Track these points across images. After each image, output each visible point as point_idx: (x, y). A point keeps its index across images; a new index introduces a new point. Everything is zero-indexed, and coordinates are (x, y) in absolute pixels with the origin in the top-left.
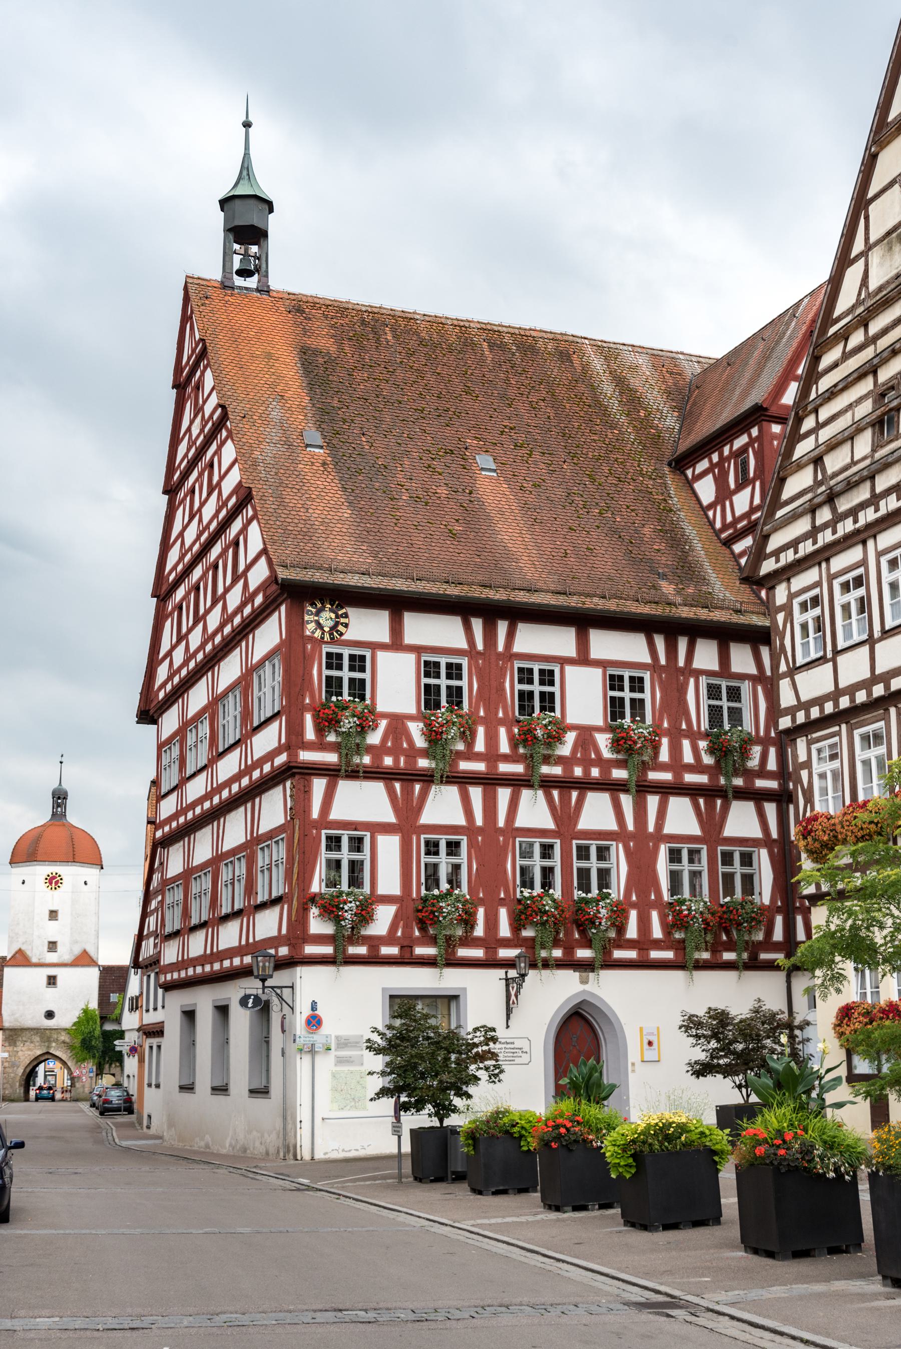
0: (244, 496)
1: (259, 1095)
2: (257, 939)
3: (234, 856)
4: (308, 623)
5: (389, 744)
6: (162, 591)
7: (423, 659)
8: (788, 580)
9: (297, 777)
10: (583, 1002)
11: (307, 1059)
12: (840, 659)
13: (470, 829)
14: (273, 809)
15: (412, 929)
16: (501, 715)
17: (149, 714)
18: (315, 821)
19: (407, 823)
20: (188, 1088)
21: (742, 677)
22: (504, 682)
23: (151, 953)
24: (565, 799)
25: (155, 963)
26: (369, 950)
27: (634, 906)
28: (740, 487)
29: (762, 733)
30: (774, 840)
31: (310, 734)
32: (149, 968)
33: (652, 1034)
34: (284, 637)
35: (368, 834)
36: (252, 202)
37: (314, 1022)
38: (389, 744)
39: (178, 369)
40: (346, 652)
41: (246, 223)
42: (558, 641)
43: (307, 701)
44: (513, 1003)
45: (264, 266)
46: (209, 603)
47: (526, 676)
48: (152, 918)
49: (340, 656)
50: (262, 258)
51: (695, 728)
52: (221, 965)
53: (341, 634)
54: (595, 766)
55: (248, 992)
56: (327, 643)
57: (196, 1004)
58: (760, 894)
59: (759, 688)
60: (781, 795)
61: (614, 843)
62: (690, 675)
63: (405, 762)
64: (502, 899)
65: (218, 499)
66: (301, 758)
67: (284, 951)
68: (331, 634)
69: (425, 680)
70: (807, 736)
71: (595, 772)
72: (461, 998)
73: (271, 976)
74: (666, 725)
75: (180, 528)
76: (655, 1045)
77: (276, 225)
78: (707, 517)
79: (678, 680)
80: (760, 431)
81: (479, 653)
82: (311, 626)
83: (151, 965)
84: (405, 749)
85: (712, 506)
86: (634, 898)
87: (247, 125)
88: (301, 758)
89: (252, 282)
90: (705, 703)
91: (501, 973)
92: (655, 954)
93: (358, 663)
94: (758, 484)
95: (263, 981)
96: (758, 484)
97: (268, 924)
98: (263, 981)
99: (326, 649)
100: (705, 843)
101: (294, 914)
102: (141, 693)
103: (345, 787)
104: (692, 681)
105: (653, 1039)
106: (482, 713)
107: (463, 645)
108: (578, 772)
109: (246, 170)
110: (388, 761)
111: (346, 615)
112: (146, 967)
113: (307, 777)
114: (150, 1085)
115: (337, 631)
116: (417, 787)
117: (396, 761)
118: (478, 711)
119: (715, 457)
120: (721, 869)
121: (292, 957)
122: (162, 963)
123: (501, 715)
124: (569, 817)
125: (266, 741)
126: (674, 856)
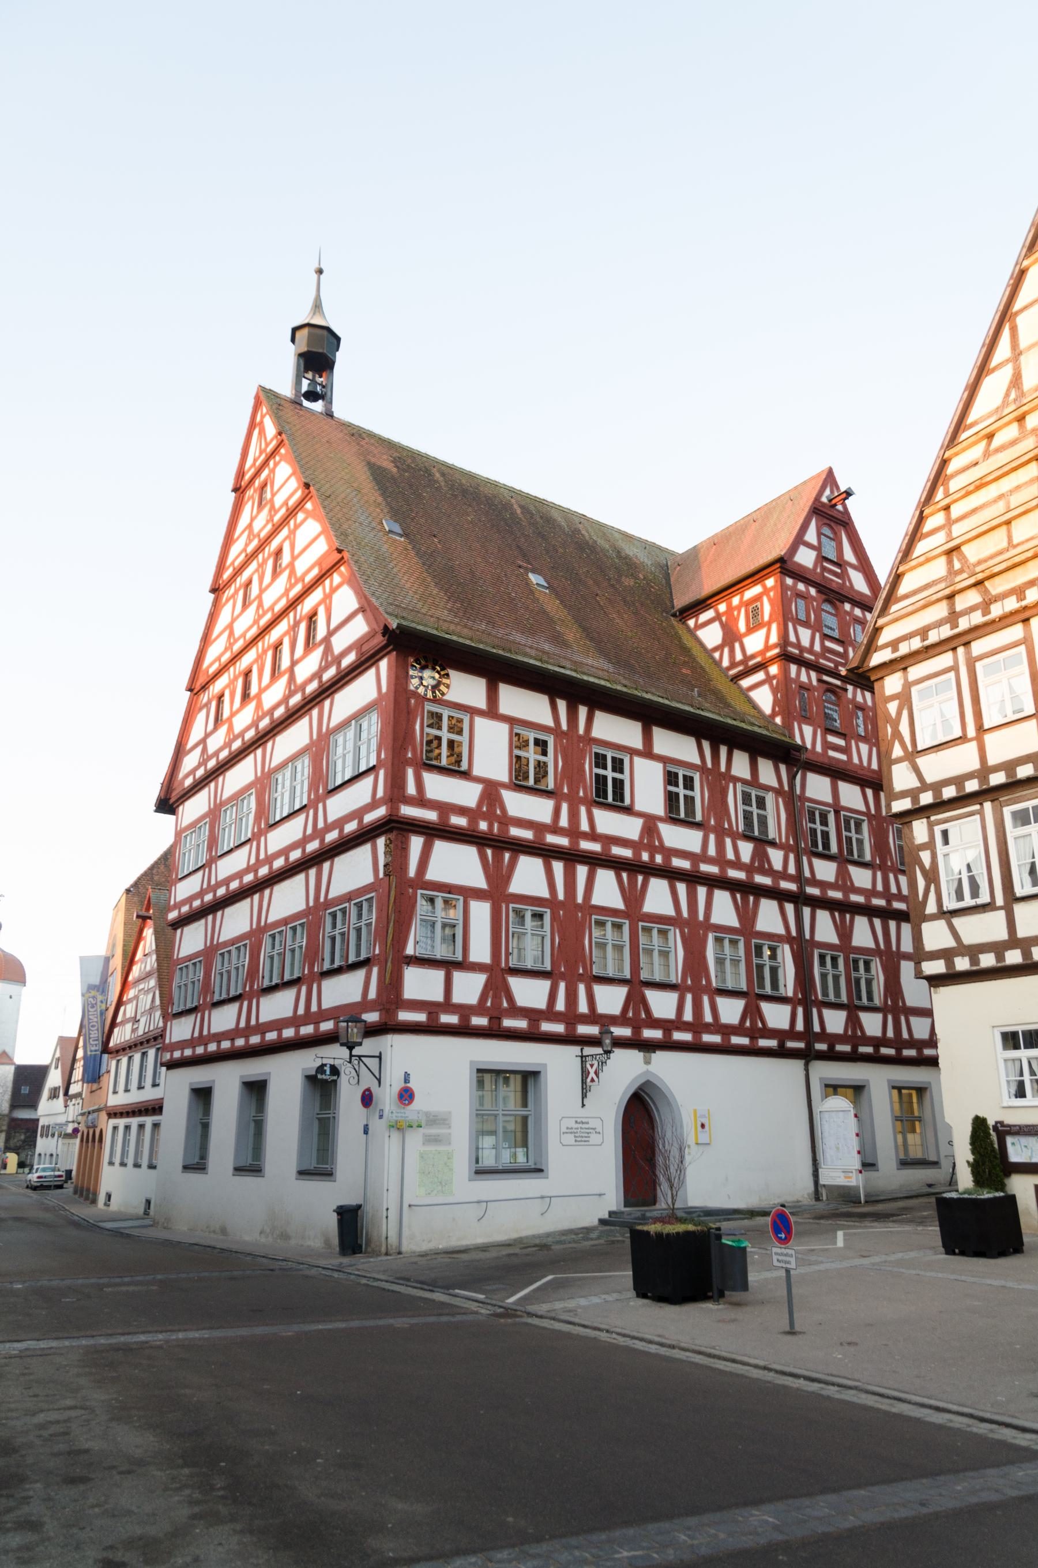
1: (243, 1173)
2: (261, 1021)
3: (286, 924)
4: (412, 677)
8: (905, 669)
9: (395, 833)
10: (648, 1083)
11: (396, 1136)
12: (988, 738)
14: (355, 870)
15: (501, 999)
16: (581, 794)
17: (167, 805)
18: (411, 880)
19: (497, 892)
20: (197, 1165)
21: (767, 788)
22: (584, 764)
23: (128, 1038)
24: (632, 881)
25: (155, 1039)
26: (460, 1019)
28: (750, 630)
29: (784, 840)
30: (794, 938)
32: (121, 1053)
33: (703, 1116)
34: (384, 690)
35: (461, 898)
36: (325, 333)
37: (406, 1096)
39: (240, 473)
41: (318, 354)
42: (624, 732)
43: (410, 755)
44: (593, 1080)
45: (329, 394)
47: (600, 761)
50: (328, 387)
52: (172, 1055)
55: (325, 1061)
56: (429, 700)
57: (214, 1081)
60: (798, 897)
61: (672, 928)
62: (730, 781)
63: (499, 829)
64: (580, 974)
65: (258, 608)
67: (372, 1017)
68: (434, 692)
70: (928, 818)
71: (659, 859)
72: (542, 1074)
73: (360, 1044)
74: (712, 822)
75: (229, 620)
76: (707, 1126)
77: (342, 358)
78: (713, 658)
79: (721, 783)
81: (563, 732)
82: (415, 682)
83: (136, 1045)
85: (719, 648)
86: (689, 982)
87: (320, 271)
89: (318, 406)
90: (741, 807)
91: (575, 1050)
95: (351, 1048)
97: (343, 990)
98: (351, 1048)
99: (429, 707)
100: (743, 935)
101: (388, 976)
103: (441, 848)
104: (731, 785)
105: (705, 1121)
106: (566, 791)
107: (550, 722)
108: (645, 857)
109: (317, 306)
110: (483, 826)
112: (117, 1051)
113: (405, 834)
114: (111, 1163)
115: (439, 691)
116: (507, 856)
117: (491, 826)
118: (563, 789)
120: (755, 961)
121: (386, 1024)
122: (167, 1041)
123: (581, 794)
124: (636, 900)
125: (360, 794)
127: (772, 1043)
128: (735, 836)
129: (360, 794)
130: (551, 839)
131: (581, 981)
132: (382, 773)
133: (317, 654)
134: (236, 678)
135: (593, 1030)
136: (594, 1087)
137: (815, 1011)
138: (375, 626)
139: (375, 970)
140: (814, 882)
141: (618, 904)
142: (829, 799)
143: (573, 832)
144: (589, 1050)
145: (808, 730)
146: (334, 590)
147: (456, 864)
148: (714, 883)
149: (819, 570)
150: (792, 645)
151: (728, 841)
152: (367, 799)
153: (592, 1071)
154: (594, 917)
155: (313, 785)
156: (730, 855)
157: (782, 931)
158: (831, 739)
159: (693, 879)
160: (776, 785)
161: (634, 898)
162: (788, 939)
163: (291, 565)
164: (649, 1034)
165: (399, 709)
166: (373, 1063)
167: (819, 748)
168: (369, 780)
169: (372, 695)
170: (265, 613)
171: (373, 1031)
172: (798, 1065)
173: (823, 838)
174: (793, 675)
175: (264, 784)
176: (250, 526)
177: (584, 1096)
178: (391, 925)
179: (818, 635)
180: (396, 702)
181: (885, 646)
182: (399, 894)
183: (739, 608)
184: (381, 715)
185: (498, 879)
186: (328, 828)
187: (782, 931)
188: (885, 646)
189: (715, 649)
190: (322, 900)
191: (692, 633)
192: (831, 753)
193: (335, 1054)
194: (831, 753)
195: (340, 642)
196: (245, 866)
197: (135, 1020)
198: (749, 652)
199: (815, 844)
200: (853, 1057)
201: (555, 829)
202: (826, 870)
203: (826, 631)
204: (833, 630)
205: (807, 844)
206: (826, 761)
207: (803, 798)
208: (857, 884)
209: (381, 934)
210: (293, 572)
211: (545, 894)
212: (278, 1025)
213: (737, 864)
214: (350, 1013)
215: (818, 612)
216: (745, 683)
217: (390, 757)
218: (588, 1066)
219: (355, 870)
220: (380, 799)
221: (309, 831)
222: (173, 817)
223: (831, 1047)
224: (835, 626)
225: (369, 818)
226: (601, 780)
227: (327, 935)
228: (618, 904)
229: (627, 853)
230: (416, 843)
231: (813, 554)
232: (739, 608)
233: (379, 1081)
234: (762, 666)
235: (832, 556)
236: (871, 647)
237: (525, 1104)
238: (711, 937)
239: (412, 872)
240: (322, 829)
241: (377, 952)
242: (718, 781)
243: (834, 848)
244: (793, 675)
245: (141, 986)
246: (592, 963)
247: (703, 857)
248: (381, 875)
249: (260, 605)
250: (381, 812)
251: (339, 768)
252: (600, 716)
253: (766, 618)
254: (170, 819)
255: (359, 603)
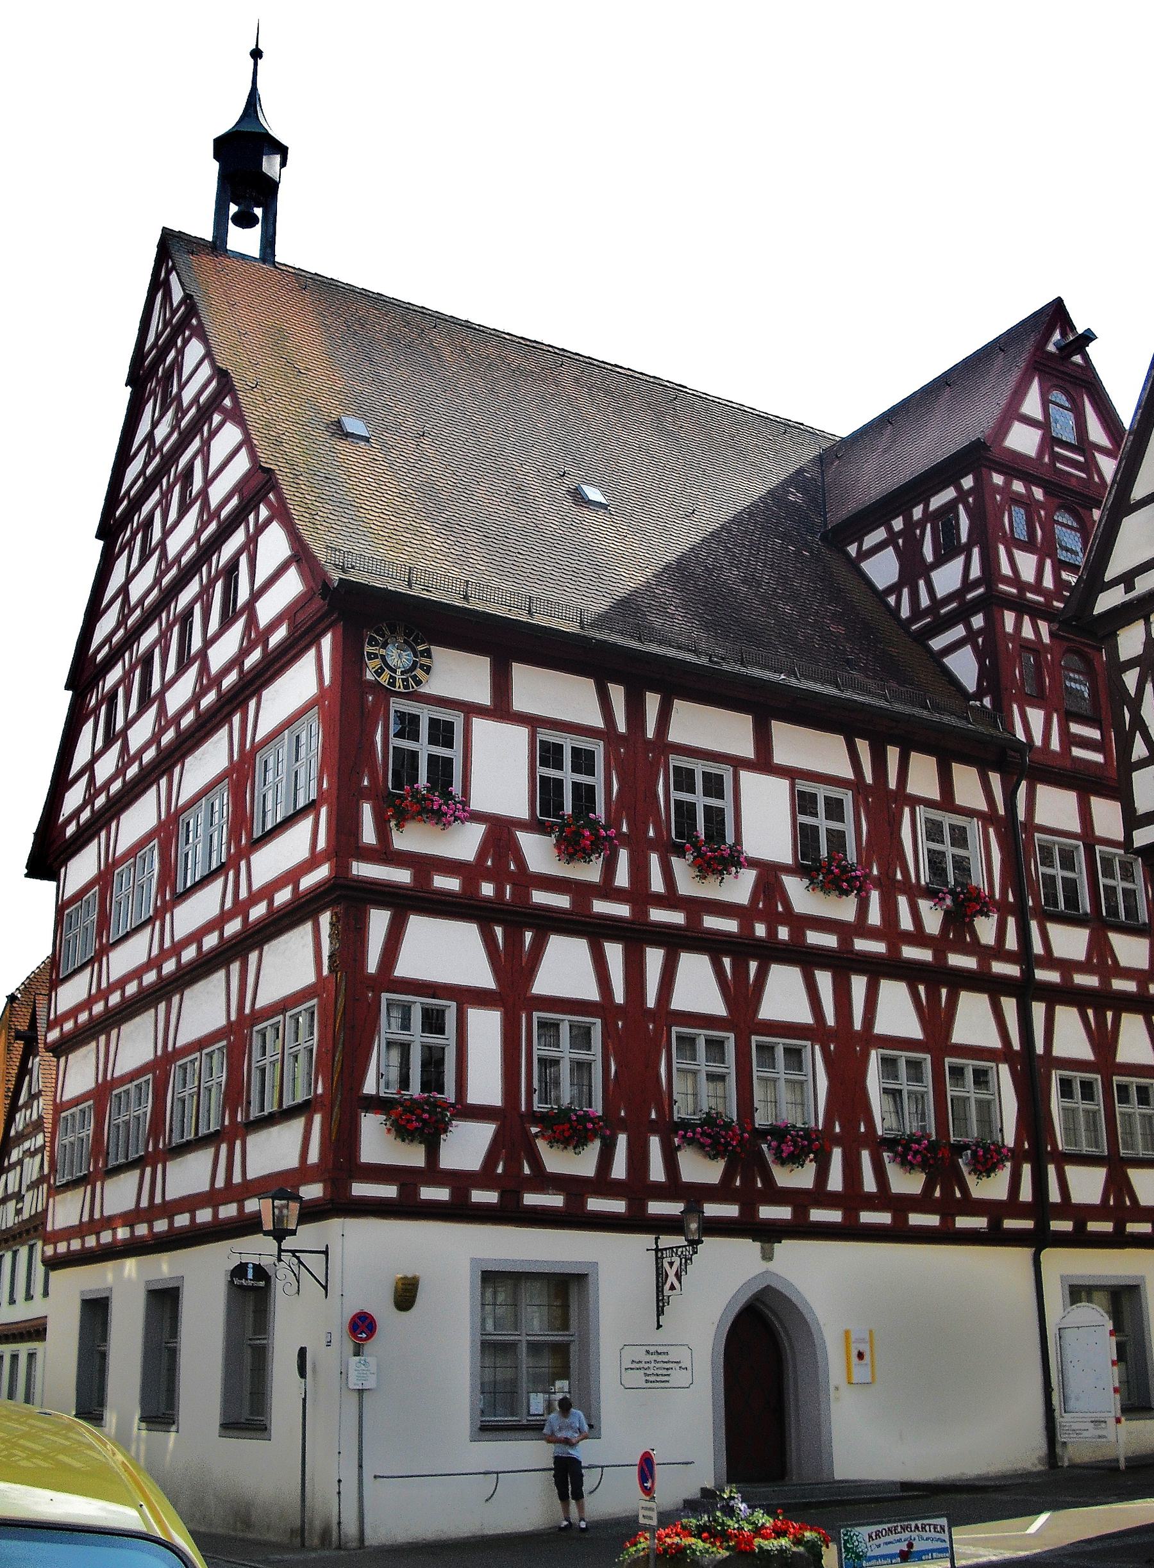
0: (259, 487)
3: (200, 1049)
5: (489, 863)
6: (84, 675)
7: (539, 737)
10: (768, 1288)
13: (604, 1008)
17: (46, 859)
19: (512, 991)
23: (10, 1224)
27: (838, 1141)
28: (941, 559)
31: (369, 836)
33: (862, 1341)
34: (327, 682)
38: (489, 863)
40: (425, 714)
41: (247, 163)
42: (730, 732)
44: (672, 1288)
46: (171, 670)
48: (11, 1175)
49: (415, 719)
51: (914, 881)
53: (419, 683)
54: (783, 924)
58: (1001, 1130)
59: (991, 830)
63: (512, 894)
66: (354, 872)
67: (312, 1191)
69: (542, 771)
72: (590, 1279)
73: (293, 1233)
75: (123, 579)
76: (867, 1357)
78: (887, 605)
79: (889, 808)
80: (976, 480)
84: (512, 872)
85: (895, 589)
88: (354, 872)
90: (924, 845)
91: (646, 1240)
92: (867, 1217)
93: (442, 733)
94: (976, 551)
96: (976, 551)
97: (276, 1150)
99: (397, 705)
102: (35, 834)
103: (418, 926)
104: (907, 810)
110: (487, 889)
111: (428, 654)
117: (500, 891)
119: (898, 524)
122: (49, 1228)
125: (292, 847)
126: (889, 1065)
127: (980, 1223)
128: (914, 892)
129: (292, 847)
130: (601, 907)
131: (655, 1132)
132: (324, 811)
133: (237, 630)
134: (132, 669)
135: (674, 1208)
136: (675, 1299)
137: (1051, 1169)
138: (312, 584)
139: (317, 1119)
140: (1050, 961)
141: (717, 1007)
142: (1076, 827)
143: (639, 895)
144: (667, 1241)
145: (1036, 716)
146: (261, 529)
147: (445, 951)
148: (879, 969)
149: (1046, 460)
150: (1006, 580)
151: (903, 901)
152: (304, 853)
153: (671, 1273)
154: (674, 1029)
155: (234, 835)
156: (906, 923)
157: (995, 1042)
158: (1075, 728)
159: (843, 964)
160: (983, 807)
161: (742, 996)
162: (1005, 1054)
163: (204, 493)
164: (767, 1212)
165: (350, 709)
166: (314, 1262)
167: (1055, 745)
168: (306, 824)
169: (310, 689)
170: (169, 568)
171: (312, 1213)
172: (1024, 1254)
173: (425, 1065)
174: (1009, 628)
175: (168, 830)
176: (150, 437)
177: (660, 1312)
178: (340, 1047)
179: (1048, 562)
180: (344, 701)
181: (1115, 582)
182: (352, 997)
183: (921, 524)
184: (326, 721)
185: (514, 970)
186: (254, 899)
187: (995, 1042)
188: (1115, 582)
189: (890, 590)
190: (247, 1011)
191: (854, 565)
192: (1077, 752)
193: (256, 1249)
194: (1077, 752)
195: (268, 609)
196: (144, 959)
197: (19, 1196)
198: (940, 593)
199: (1052, 899)
200: (1119, 1240)
201: (607, 891)
202: (1070, 942)
203: (1063, 555)
204: (1076, 554)
205: (1027, 901)
206: (1068, 764)
207: (1030, 826)
208: (1124, 962)
209: (323, 1063)
210: (206, 503)
211: (592, 994)
212: (190, 1203)
213: (919, 938)
214: (279, 1186)
215: (1049, 526)
216: (937, 643)
217: (335, 786)
218: (666, 1265)
219: (291, 965)
220: (321, 852)
221: (228, 904)
222: (53, 885)
223: (1080, 1226)
224: (1078, 547)
225: (307, 882)
226: (686, 811)
227: (254, 1065)
228: (717, 1007)
229: (730, 925)
230: (379, 921)
231: (1036, 435)
232: (921, 524)
233: (325, 1288)
234: (962, 615)
235: (1070, 437)
236: (1094, 582)
237: (565, 1326)
238: (874, 1056)
239: (372, 967)
240: (244, 901)
241: (320, 1091)
242: (884, 804)
243: (1086, 904)
244: (1009, 628)
245: (27, 1145)
246: (672, 1102)
247: (860, 927)
248: (325, 972)
249: (164, 555)
250: (323, 872)
251: (269, 805)
252: (682, 709)
253: (964, 539)
254: (48, 887)
255: (292, 548)
